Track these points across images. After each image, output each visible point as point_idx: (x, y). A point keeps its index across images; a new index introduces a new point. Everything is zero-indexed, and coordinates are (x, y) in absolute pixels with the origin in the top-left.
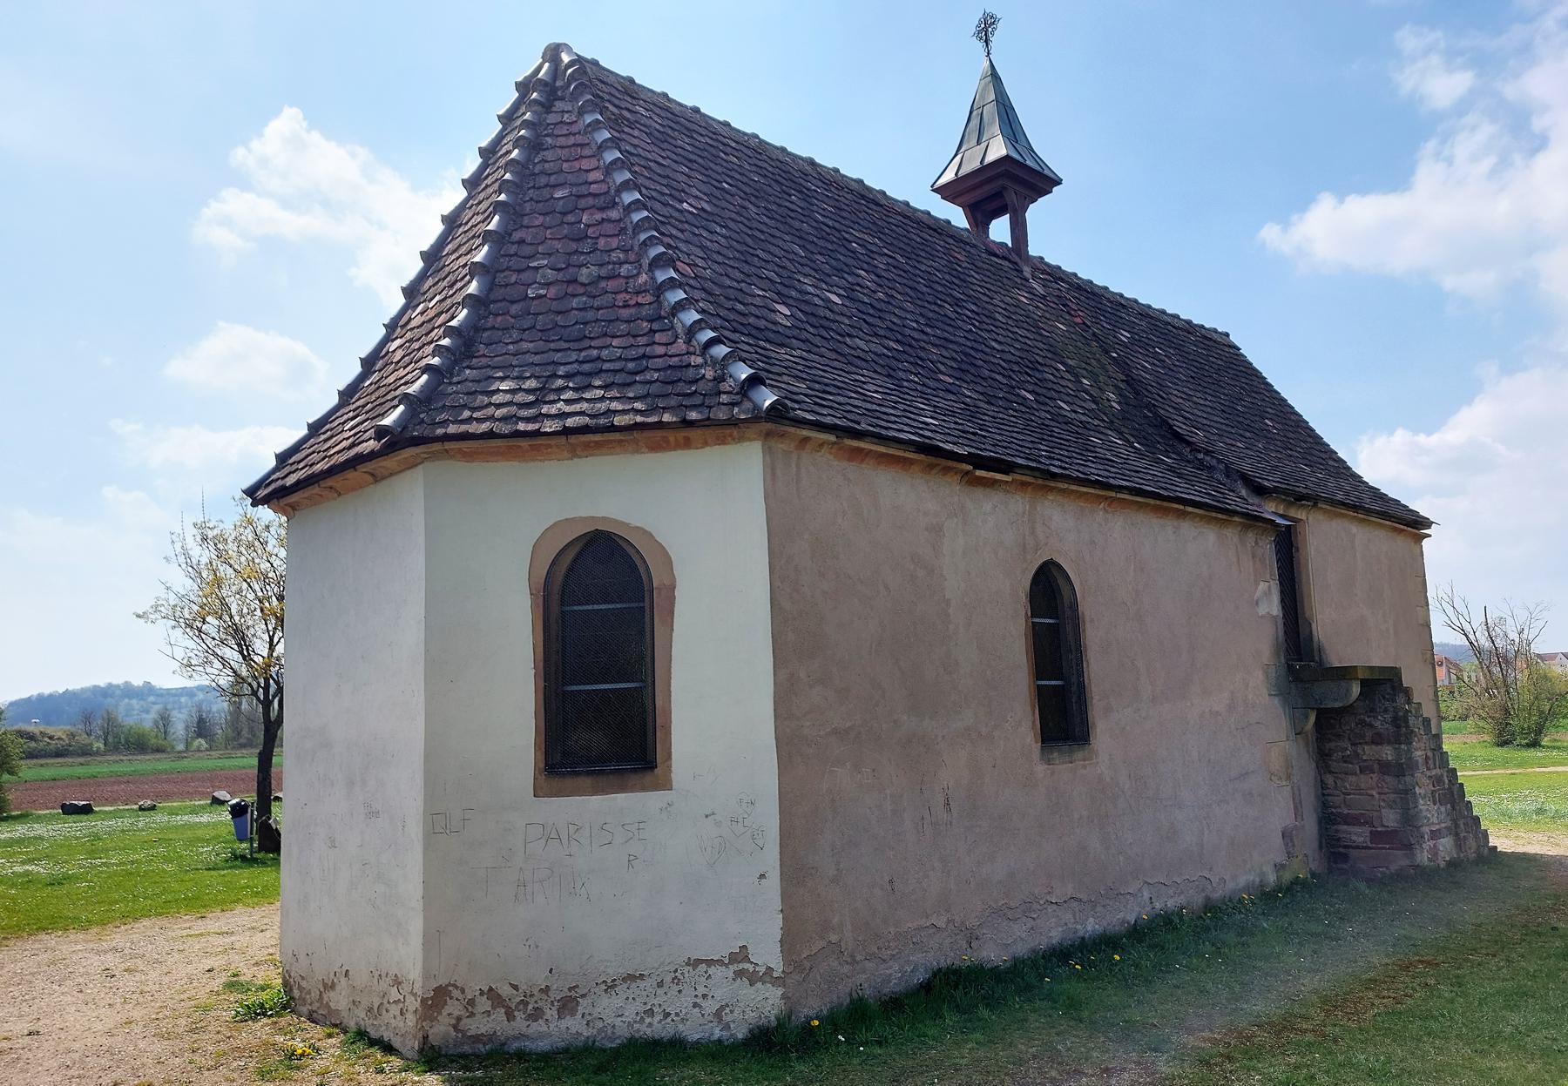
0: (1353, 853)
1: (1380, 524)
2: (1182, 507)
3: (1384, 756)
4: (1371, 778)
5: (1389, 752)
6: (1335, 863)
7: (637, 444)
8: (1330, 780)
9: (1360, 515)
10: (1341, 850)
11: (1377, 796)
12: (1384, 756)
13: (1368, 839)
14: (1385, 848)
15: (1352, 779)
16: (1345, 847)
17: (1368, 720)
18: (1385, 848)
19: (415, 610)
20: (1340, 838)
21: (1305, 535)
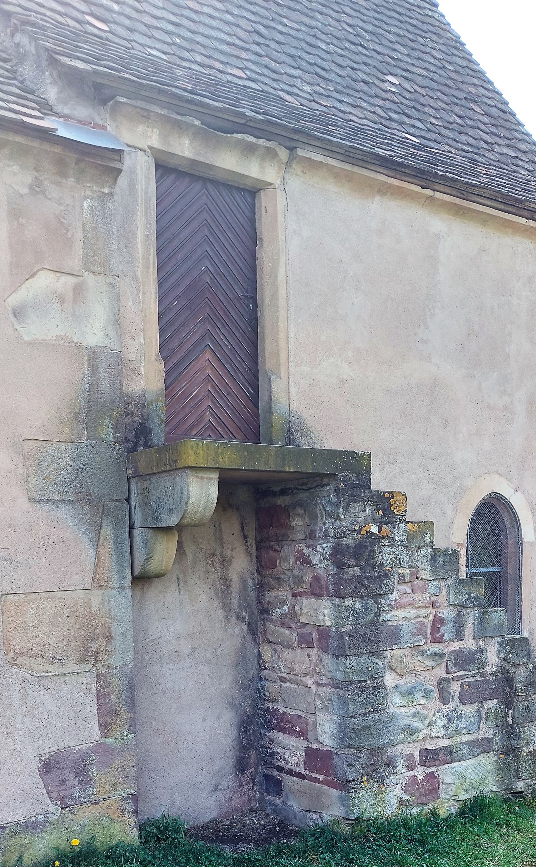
0: (288, 781)
1: (508, 224)
2: (251, 139)
3: (321, 618)
4: (309, 656)
5: (326, 612)
6: (268, 793)
7: (174, 828)
8: (267, 652)
9: (438, 195)
10: (275, 773)
11: (314, 688)
12: (321, 618)
13: (302, 763)
14: (317, 780)
15: (287, 654)
16: (280, 769)
17: (306, 551)
18: (317, 780)
19: (349, 169)
20: (273, 752)
21: (275, 216)
